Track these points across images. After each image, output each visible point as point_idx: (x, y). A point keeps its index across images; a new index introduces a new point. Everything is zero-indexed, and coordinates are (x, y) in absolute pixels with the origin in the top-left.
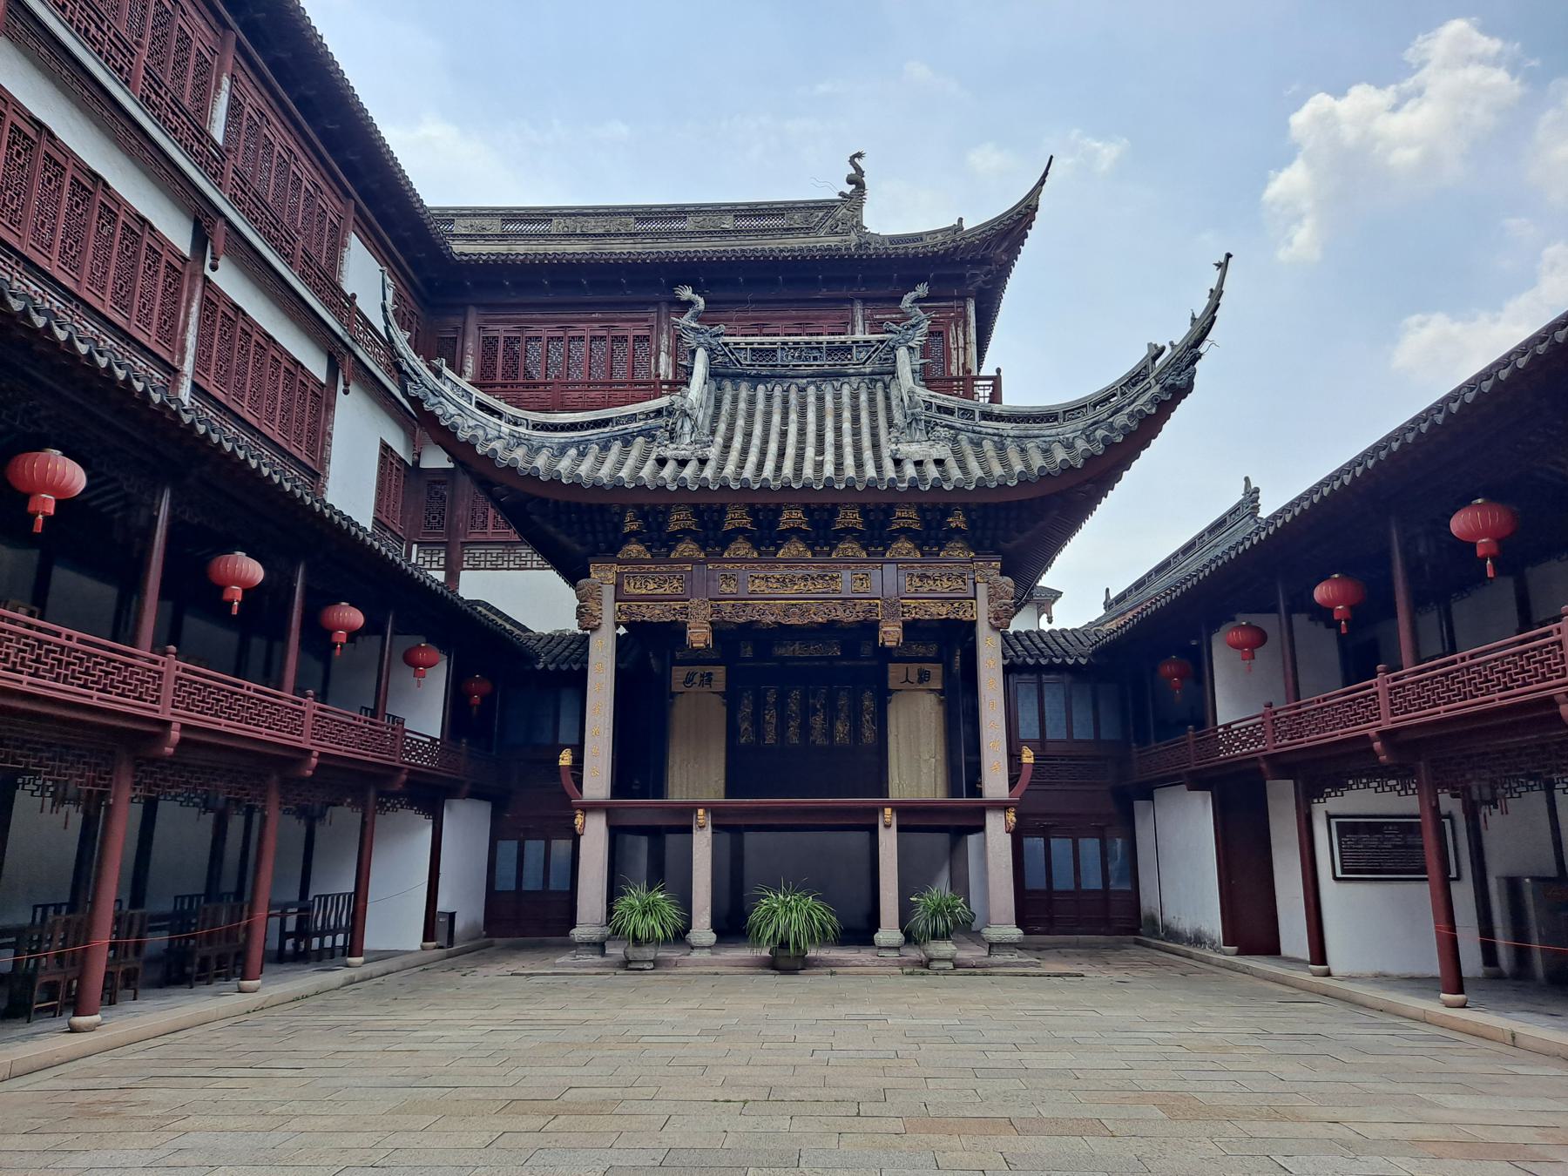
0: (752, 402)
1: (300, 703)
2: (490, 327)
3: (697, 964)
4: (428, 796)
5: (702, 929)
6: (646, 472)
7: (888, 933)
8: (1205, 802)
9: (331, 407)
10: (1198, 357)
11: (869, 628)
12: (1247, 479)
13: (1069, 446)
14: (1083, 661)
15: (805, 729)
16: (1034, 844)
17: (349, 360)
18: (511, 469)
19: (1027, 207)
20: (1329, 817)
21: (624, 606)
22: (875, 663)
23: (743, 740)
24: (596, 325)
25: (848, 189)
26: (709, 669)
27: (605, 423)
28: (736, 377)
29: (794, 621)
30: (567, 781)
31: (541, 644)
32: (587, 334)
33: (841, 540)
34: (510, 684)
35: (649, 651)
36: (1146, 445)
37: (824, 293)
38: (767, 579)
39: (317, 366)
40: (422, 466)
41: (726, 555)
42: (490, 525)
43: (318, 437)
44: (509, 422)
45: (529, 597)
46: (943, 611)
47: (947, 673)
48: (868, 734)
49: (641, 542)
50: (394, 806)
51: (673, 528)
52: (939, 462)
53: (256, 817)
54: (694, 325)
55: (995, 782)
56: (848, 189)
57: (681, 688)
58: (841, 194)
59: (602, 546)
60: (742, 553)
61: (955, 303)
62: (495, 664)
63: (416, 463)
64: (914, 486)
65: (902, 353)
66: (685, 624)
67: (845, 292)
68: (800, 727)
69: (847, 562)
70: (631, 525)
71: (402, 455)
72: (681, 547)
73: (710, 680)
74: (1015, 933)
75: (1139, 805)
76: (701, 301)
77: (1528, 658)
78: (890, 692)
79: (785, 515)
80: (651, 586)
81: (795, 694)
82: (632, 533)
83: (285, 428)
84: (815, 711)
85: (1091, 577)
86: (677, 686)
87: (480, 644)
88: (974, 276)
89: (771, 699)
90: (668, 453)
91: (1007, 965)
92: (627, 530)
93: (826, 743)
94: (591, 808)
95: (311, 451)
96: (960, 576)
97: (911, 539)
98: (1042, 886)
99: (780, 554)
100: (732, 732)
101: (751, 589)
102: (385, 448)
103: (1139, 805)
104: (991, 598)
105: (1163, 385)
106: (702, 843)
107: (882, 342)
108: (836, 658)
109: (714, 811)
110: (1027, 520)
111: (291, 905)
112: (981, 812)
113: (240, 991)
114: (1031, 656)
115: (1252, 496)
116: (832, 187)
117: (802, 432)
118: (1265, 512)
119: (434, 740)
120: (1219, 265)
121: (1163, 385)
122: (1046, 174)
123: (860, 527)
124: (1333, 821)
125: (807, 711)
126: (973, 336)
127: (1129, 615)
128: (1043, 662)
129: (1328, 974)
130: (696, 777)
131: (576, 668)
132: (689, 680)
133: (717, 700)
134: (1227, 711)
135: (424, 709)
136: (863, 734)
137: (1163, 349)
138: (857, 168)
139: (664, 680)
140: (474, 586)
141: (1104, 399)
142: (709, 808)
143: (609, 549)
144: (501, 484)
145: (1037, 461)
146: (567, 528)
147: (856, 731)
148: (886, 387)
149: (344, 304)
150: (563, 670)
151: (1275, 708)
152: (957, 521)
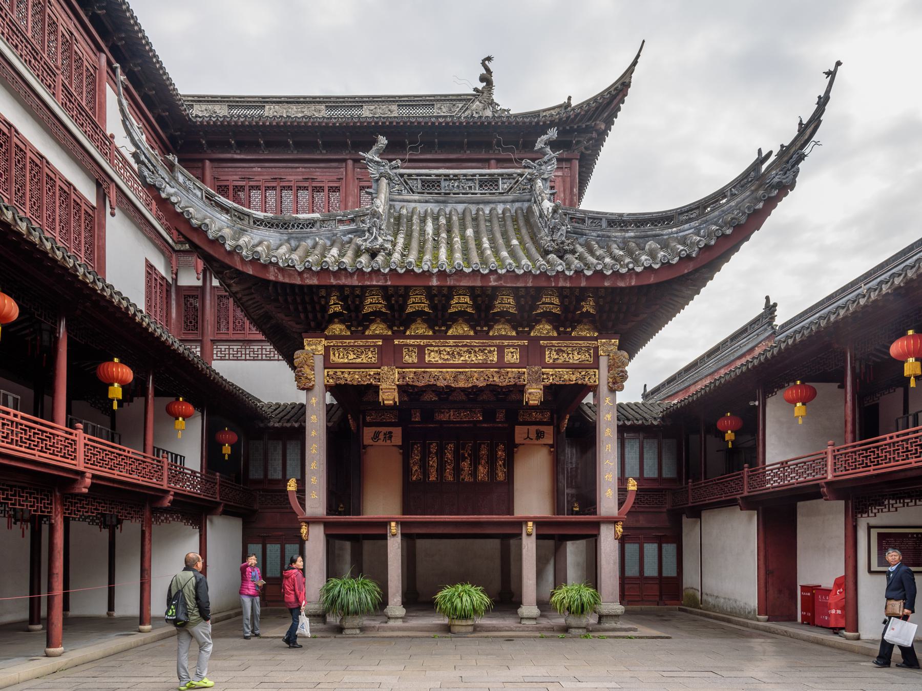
1: (71, 434)
3: (393, 629)
4: (194, 512)
5: (395, 606)
6: (347, 260)
7: (529, 609)
9: (102, 227)
10: (802, 157)
12: (767, 298)
15: (457, 470)
16: (632, 549)
20: (870, 528)
21: (331, 372)
22: (506, 425)
23: (414, 478)
25: (481, 86)
29: (461, 384)
31: (270, 410)
33: (497, 322)
34: (248, 436)
35: (353, 404)
36: (747, 238)
39: (87, 191)
41: (408, 333)
43: (95, 249)
45: (262, 377)
48: (501, 476)
49: (342, 322)
50: (166, 519)
51: (367, 310)
53: (45, 528)
55: (608, 501)
56: (481, 86)
57: (370, 442)
58: (476, 90)
59: (313, 324)
60: (420, 332)
63: (175, 280)
66: (378, 387)
68: (454, 469)
70: (335, 307)
71: (164, 274)
72: (373, 327)
73: (390, 437)
74: (619, 608)
78: (517, 446)
80: (352, 356)
82: (336, 315)
84: (464, 459)
86: (367, 440)
87: (226, 409)
88: (578, 142)
91: (614, 630)
92: (331, 311)
94: (311, 522)
97: (549, 322)
98: (655, 573)
100: (406, 471)
102: (150, 267)
104: (610, 368)
105: (766, 184)
106: (394, 547)
108: (480, 422)
110: (632, 309)
112: (597, 525)
113: (47, 655)
115: (770, 309)
116: (469, 84)
118: (779, 321)
119: (194, 472)
121: (766, 184)
122: (638, 56)
124: (874, 532)
125: (458, 458)
129: (858, 638)
130: (382, 504)
131: (296, 425)
132: (376, 437)
139: (359, 436)
143: (318, 327)
146: (287, 310)
147: (492, 472)
149: (106, 142)
150: (289, 427)
152: (588, 307)
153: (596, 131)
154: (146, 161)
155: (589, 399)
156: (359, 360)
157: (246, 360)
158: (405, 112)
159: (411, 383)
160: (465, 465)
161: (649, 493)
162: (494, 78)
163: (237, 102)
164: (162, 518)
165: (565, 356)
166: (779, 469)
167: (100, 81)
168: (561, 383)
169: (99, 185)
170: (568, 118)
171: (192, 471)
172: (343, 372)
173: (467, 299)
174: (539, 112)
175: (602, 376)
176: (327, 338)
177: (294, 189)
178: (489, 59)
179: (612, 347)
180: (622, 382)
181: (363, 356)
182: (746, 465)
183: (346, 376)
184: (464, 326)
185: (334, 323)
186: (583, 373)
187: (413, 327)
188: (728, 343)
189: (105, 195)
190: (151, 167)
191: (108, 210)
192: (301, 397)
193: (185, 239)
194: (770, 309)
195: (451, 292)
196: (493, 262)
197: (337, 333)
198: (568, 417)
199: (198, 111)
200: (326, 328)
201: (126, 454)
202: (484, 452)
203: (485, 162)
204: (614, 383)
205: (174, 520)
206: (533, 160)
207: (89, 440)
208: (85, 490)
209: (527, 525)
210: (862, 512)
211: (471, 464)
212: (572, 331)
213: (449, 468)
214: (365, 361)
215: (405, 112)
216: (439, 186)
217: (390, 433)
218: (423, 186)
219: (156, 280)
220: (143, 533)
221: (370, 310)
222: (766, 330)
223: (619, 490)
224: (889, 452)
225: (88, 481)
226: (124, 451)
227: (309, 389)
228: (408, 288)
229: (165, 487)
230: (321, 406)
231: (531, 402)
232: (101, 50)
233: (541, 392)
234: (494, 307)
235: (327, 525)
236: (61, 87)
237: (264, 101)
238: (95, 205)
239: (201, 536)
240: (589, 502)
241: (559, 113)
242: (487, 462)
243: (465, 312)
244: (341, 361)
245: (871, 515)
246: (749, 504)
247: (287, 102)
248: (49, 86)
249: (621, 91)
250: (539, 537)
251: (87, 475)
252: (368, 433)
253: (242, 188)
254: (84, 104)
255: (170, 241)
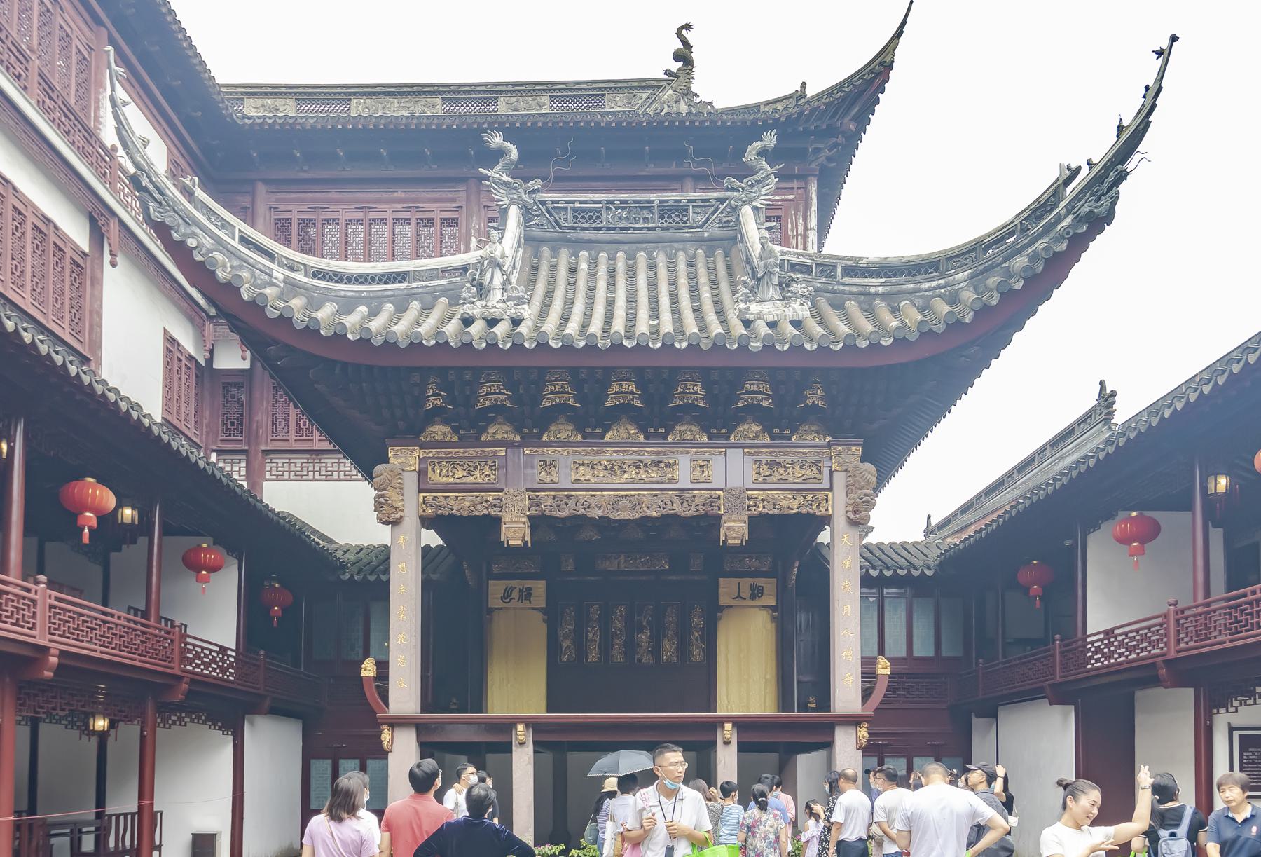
0: (573, 270)
1: (29, 590)
2: (282, 207)
4: (223, 706)
6: (451, 328)
8: (1066, 716)
9: (97, 281)
10: (1123, 176)
11: (711, 522)
12: (1102, 383)
13: (953, 299)
14: (929, 573)
15: (631, 647)
17: (114, 227)
18: (284, 321)
19: (882, 64)
20: (1231, 729)
23: (565, 659)
24: (399, 206)
25: (675, 66)
26: (528, 583)
27: (400, 277)
28: (556, 244)
29: (624, 515)
30: (371, 693)
32: (389, 216)
33: (679, 420)
35: (466, 557)
36: (1047, 296)
37: (651, 169)
38: (592, 466)
39: (76, 231)
40: (216, 366)
41: (545, 438)
42: (292, 432)
43: (85, 314)
44: (281, 265)
45: (333, 505)
46: (795, 504)
47: (781, 592)
48: (697, 655)
49: (445, 422)
51: (483, 403)
52: (796, 323)
54: (505, 178)
55: (846, 693)
56: (675, 66)
57: (500, 604)
58: (667, 72)
60: (563, 436)
61: (795, 184)
62: (289, 570)
63: (210, 361)
64: (768, 348)
65: (747, 211)
67: (673, 169)
69: (686, 446)
71: (193, 353)
75: (977, 723)
76: (514, 152)
77: (1242, 611)
78: (722, 609)
79: (614, 389)
81: (621, 610)
82: (436, 411)
83: (39, 293)
84: (641, 629)
85: (933, 489)
86: (495, 601)
88: (817, 151)
89: (595, 615)
90: (476, 311)
92: (429, 406)
93: (653, 661)
94: (397, 723)
95: (77, 332)
96: (816, 463)
97: (757, 420)
99: (608, 438)
101: (574, 476)
102: (171, 341)
103: (977, 723)
104: (849, 488)
105: (1076, 213)
107: (722, 201)
109: (534, 725)
111: (89, 824)
112: (714, 726)
114: (874, 568)
115: (1107, 399)
116: (655, 62)
117: (632, 301)
118: (1120, 417)
119: (223, 650)
120: (1160, 53)
121: (1076, 213)
123: (700, 403)
124: (1236, 734)
126: (813, 221)
127: (971, 531)
128: (887, 573)
130: (517, 692)
132: (507, 595)
133: (539, 616)
134: (1100, 615)
135: (213, 617)
136: (691, 652)
137: (1079, 169)
138: (685, 42)
139: (482, 592)
140: (283, 495)
141: (998, 238)
142: (531, 724)
143: (411, 434)
144: (276, 342)
145: (914, 316)
148: (726, 254)
150: (366, 581)
151: (1180, 606)
153: (843, 133)
154: (151, 187)
155: (824, 537)
156: (471, 479)
157: (314, 480)
158: (563, 107)
159: (547, 513)
160: (643, 638)
161: (909, 674)
162: (695, 56)
163: (310, 93)
164: (174, 718)
165: (782, 471)
166: (1102, 640)
167: (97, 67)
168: (776, 511)
169: (93, 222)
170: (800, 114)
171: (221, 647)
172: (446, 497)
173: (633, 387)
174: (757, 106)
175: (838, 505)
176: (423, 446)
177: (390, 222)
178: (687, 27)
179: (852, 458)
180: (867, 510)
181: (477, 473)
182: (1057, 636)
183: (452, 502)
184: (629, 427)
185: (434, 423)
186: (809, 498)
187: (553, 428)
188: (1047, 452)
189: (102, 236)
190: (157, 196)
191: (107, 258)
192: (381, 535)
193: (218, 302)
194: (1107, 399)
195: (608, 375)
196: (692, 327)
197: (438, 438)
198: (797, 564)
199: (252, 109)
200: (422, 430)
201: (115, 620)
202: (671, 618)
203: (674, 181)
204: (855, 512)
205: (192, 721)
206: (741, 179)
207: (57, 599)
208: (48, 674)
209: (723, 727)
210: (1218, 707)
211: (651, 637)
212: (792, 434)
213: (618, 642)
214: (479, 481)
215: (563, 107)
216: (598, 218)
217: (530, 589)
218: (576, 217)
219: (180, 360)
220: (143, 737)
221: (487, 404)
222: (1100, 432)
223: (864, 675)
224: (1251, 614)
225: (54, 660)
226: (113, 616)
227: (395, 523)
228: (543, 371)
229: (176, 671)
230: (413, 547)
231: (730, 541)
232: (99, 22)
233: (746, 526)
234: (673, 398)
235: (420, 727)
236: (37, 78)
237: (346, 93)
238: (87, 250)
239: (235, 746)
240: (822, 689)
241: (786, 108)
242: (676, 634)
243: (694, 406)
244: (445, 480)
245: (1231, 709)
246: (1059, 696)
247: (385, 94)
248: (19, 77)
249: (878, 74)
250: (742, 748)
251: (52, 651)
252: (496, 588)
253: (312, 222)
254: (72, 102)
255: (202, 302)
